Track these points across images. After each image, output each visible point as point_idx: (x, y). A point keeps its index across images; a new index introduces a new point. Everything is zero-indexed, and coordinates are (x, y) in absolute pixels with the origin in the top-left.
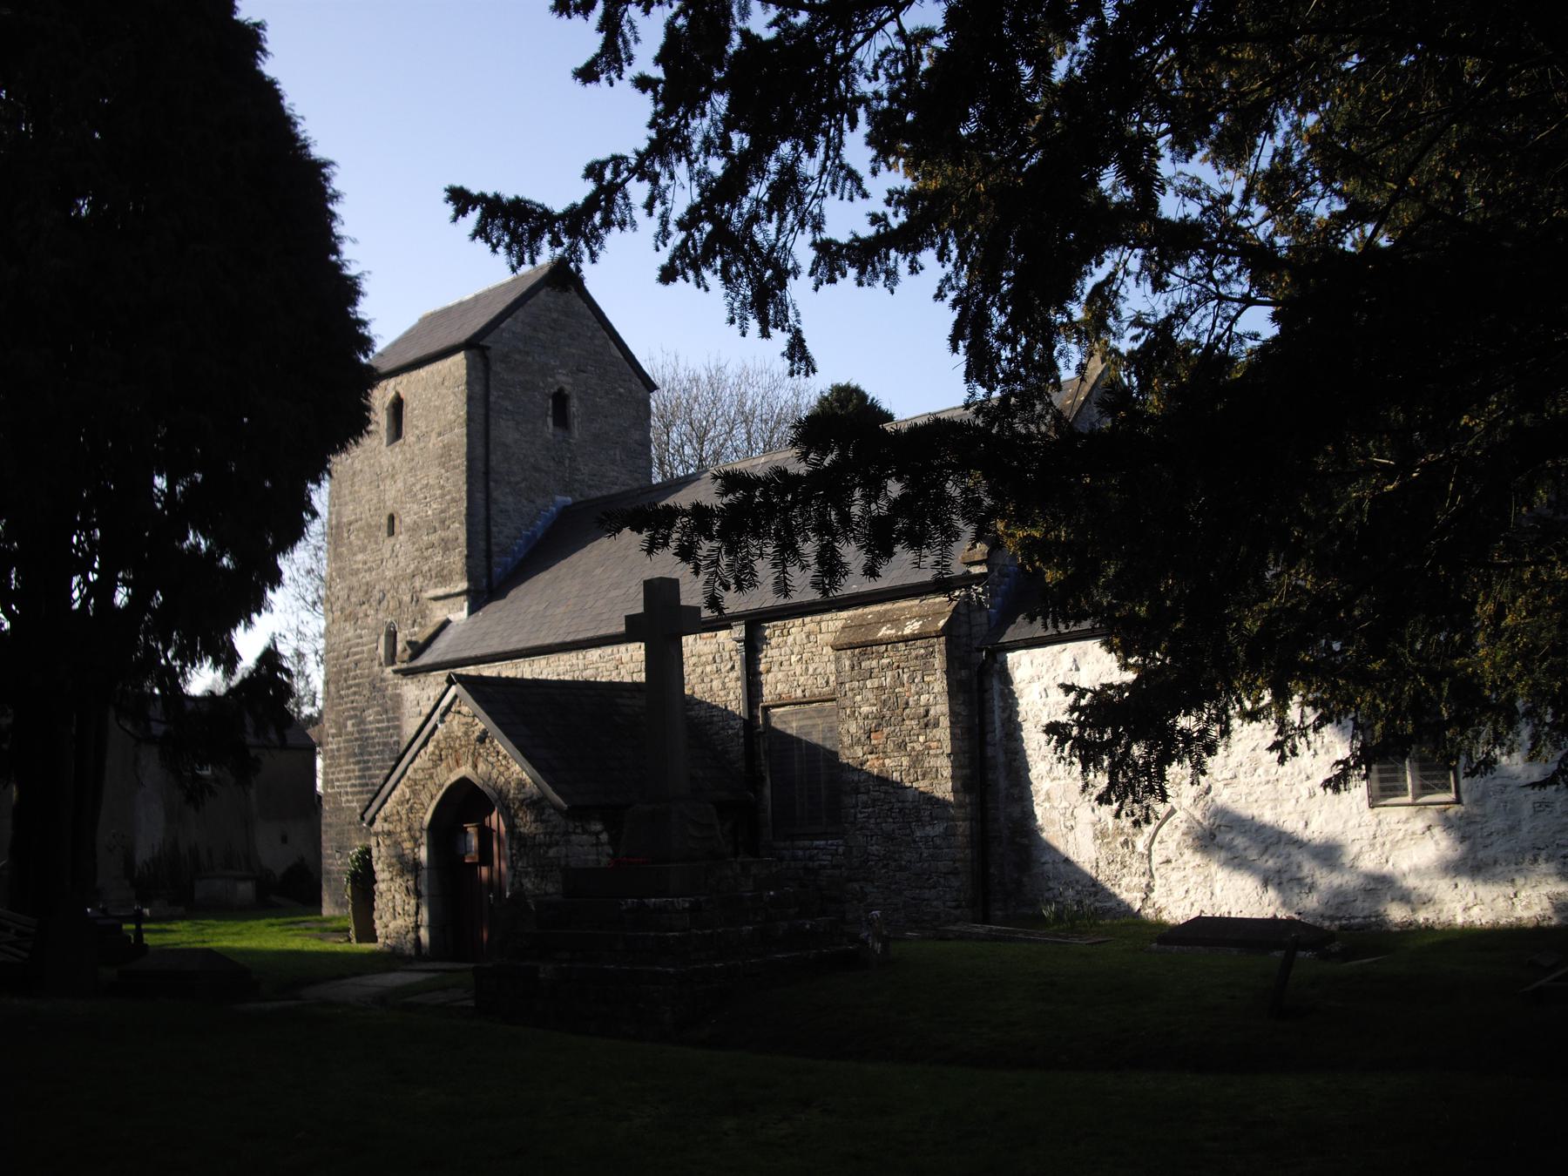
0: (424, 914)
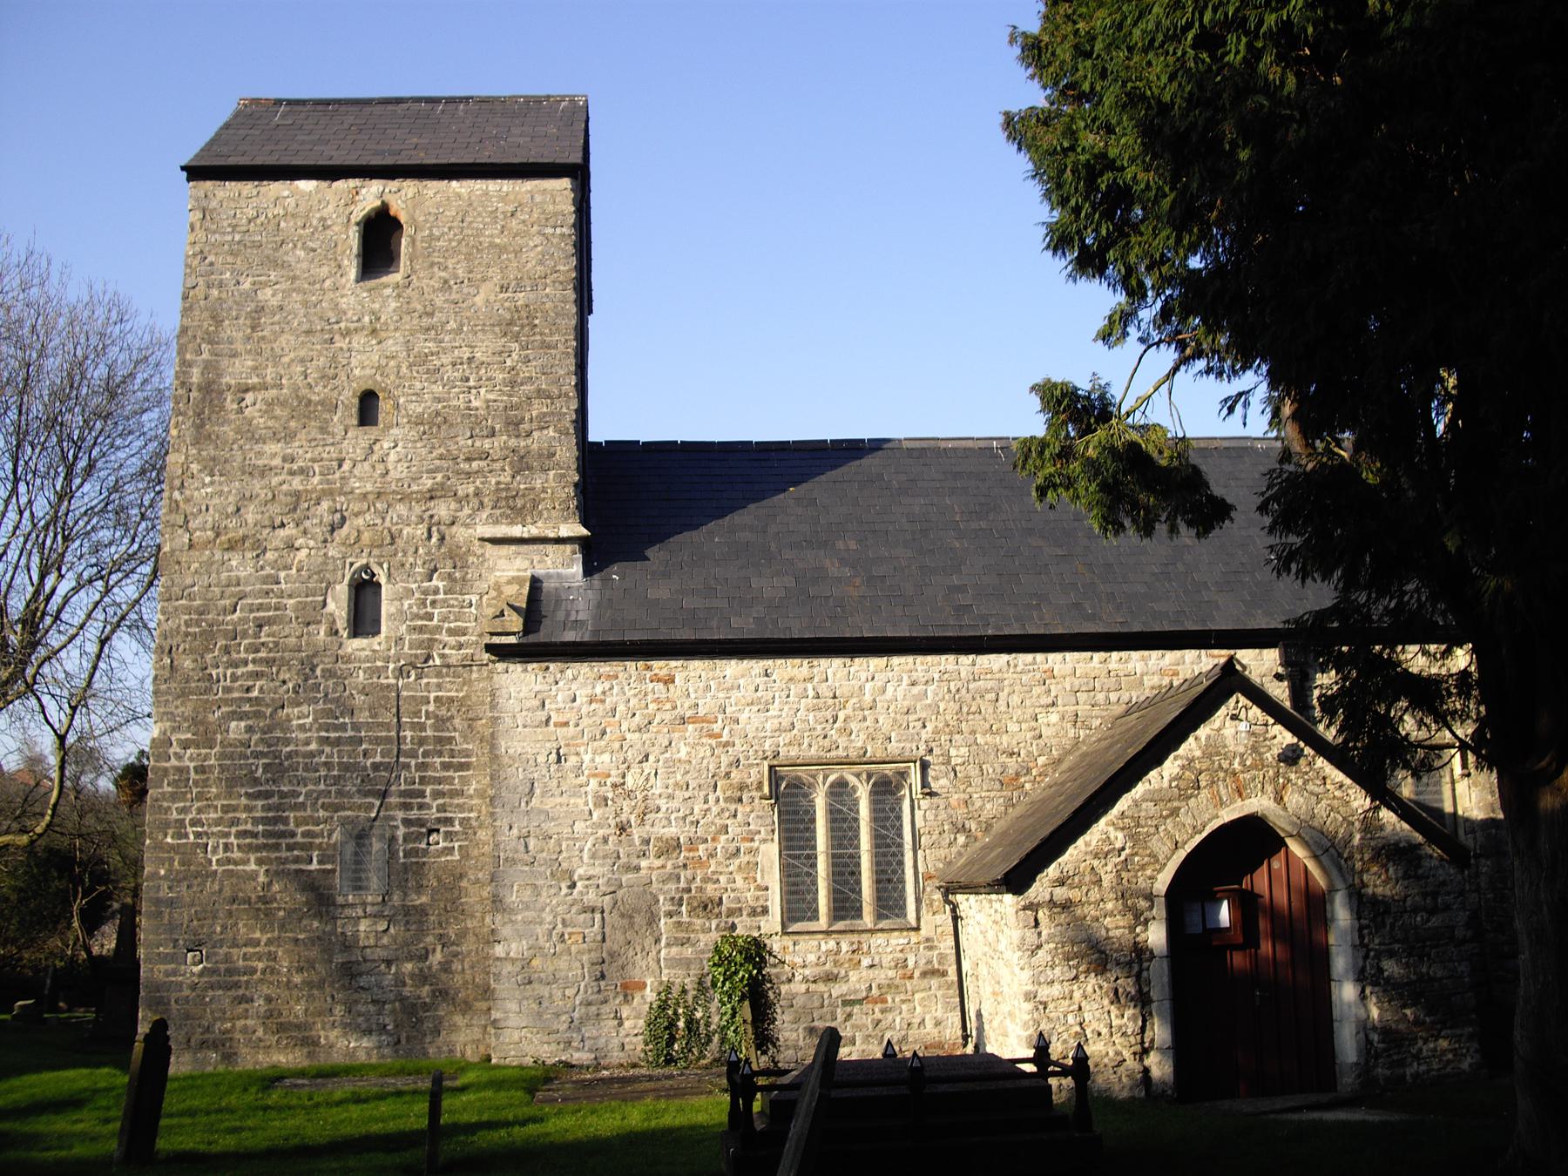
0: (1160, 1032)
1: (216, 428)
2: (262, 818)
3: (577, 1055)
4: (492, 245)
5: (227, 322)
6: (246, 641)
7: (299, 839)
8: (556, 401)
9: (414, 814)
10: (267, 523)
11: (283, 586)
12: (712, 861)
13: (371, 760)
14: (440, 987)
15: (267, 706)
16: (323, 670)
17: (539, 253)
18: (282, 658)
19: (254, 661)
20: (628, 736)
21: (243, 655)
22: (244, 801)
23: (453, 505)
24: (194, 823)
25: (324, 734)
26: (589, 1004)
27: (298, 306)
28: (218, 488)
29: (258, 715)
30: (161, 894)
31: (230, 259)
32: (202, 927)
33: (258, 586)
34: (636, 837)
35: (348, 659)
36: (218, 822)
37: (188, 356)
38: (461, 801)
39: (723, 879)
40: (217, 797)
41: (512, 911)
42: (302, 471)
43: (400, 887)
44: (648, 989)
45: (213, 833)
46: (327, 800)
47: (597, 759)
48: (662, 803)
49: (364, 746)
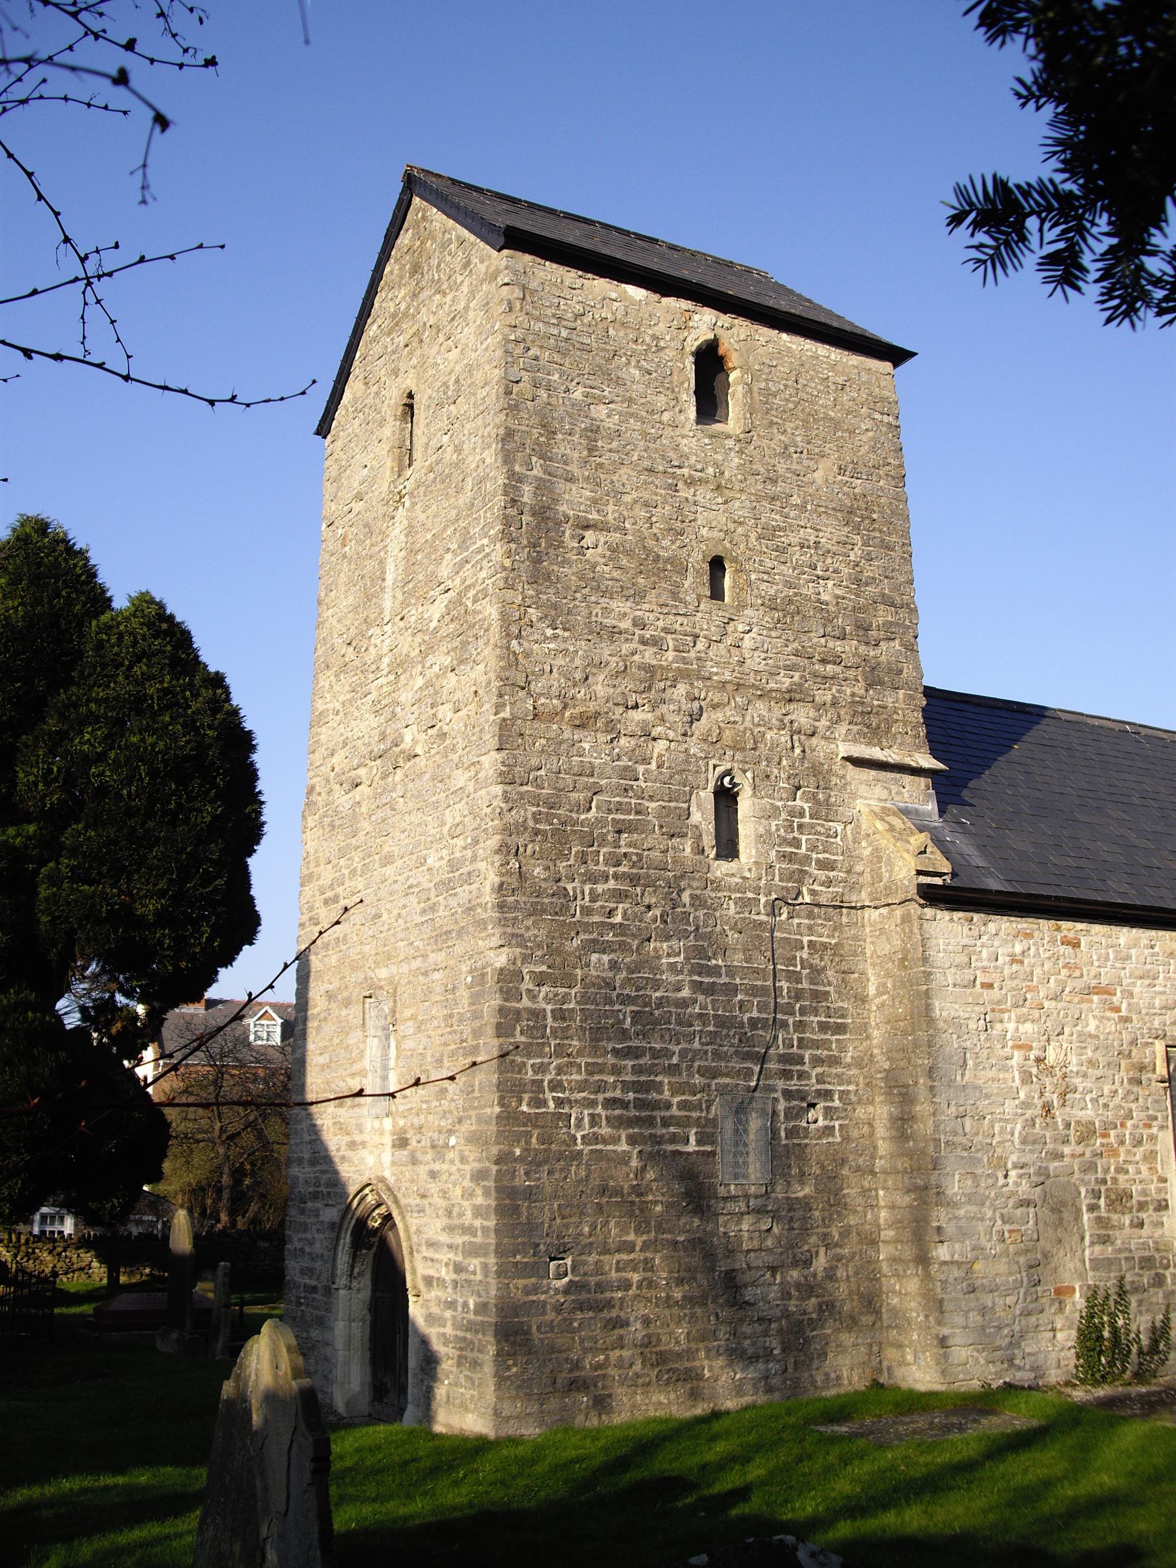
1: (556, 568)
2: (634, 1082)
3: (1019, 1375)
4: (826, 418)
5: (560, 436)
6: (605, 850)
7: (674, 1111)
8: (900, 611)
9: (794, 1084)
10: (619, 700)
11: (644, 785)
12: (1122, 1149)
13: (747, 1015)
14: (826, 1299)
15: (634, 936)
16: (692, 896)
17: (871, 439)
18: (648, 876)
19: (616, 877)
20: (1046, 1004)
21: (602, 867)
22: (611, 1059)
23: (812, 713)
24: (556, 1086)
25: (696, 978)
26: (1029, 1314)
27: (636, 435)
28: (563, 646)
29: (623, 947)
30: (517, 1182)
31: (557, 358)
32: (567, 1226)
33: (614, 780)
34: (1059, 1120)
35: (717, 885)
36: (582, 1086)
37: (517, 468)
38: (840, 1070)
39: (1131, 1169)
40: (580, 1053)
41: (955, 1205)
42: (655, 642)
43: (783, 1175)
44: (1077, 1294)
45: (576, 1101)
46: (703, 1063)
47: (1022, 1028)
48: (1077, 1081)
49: (739, 997)
